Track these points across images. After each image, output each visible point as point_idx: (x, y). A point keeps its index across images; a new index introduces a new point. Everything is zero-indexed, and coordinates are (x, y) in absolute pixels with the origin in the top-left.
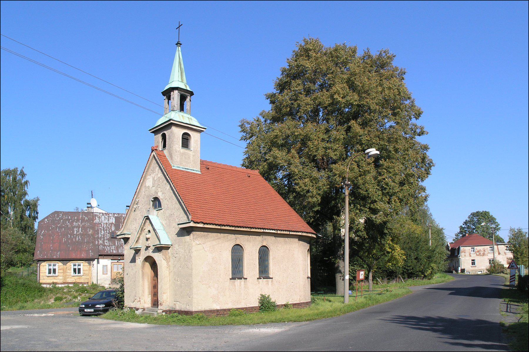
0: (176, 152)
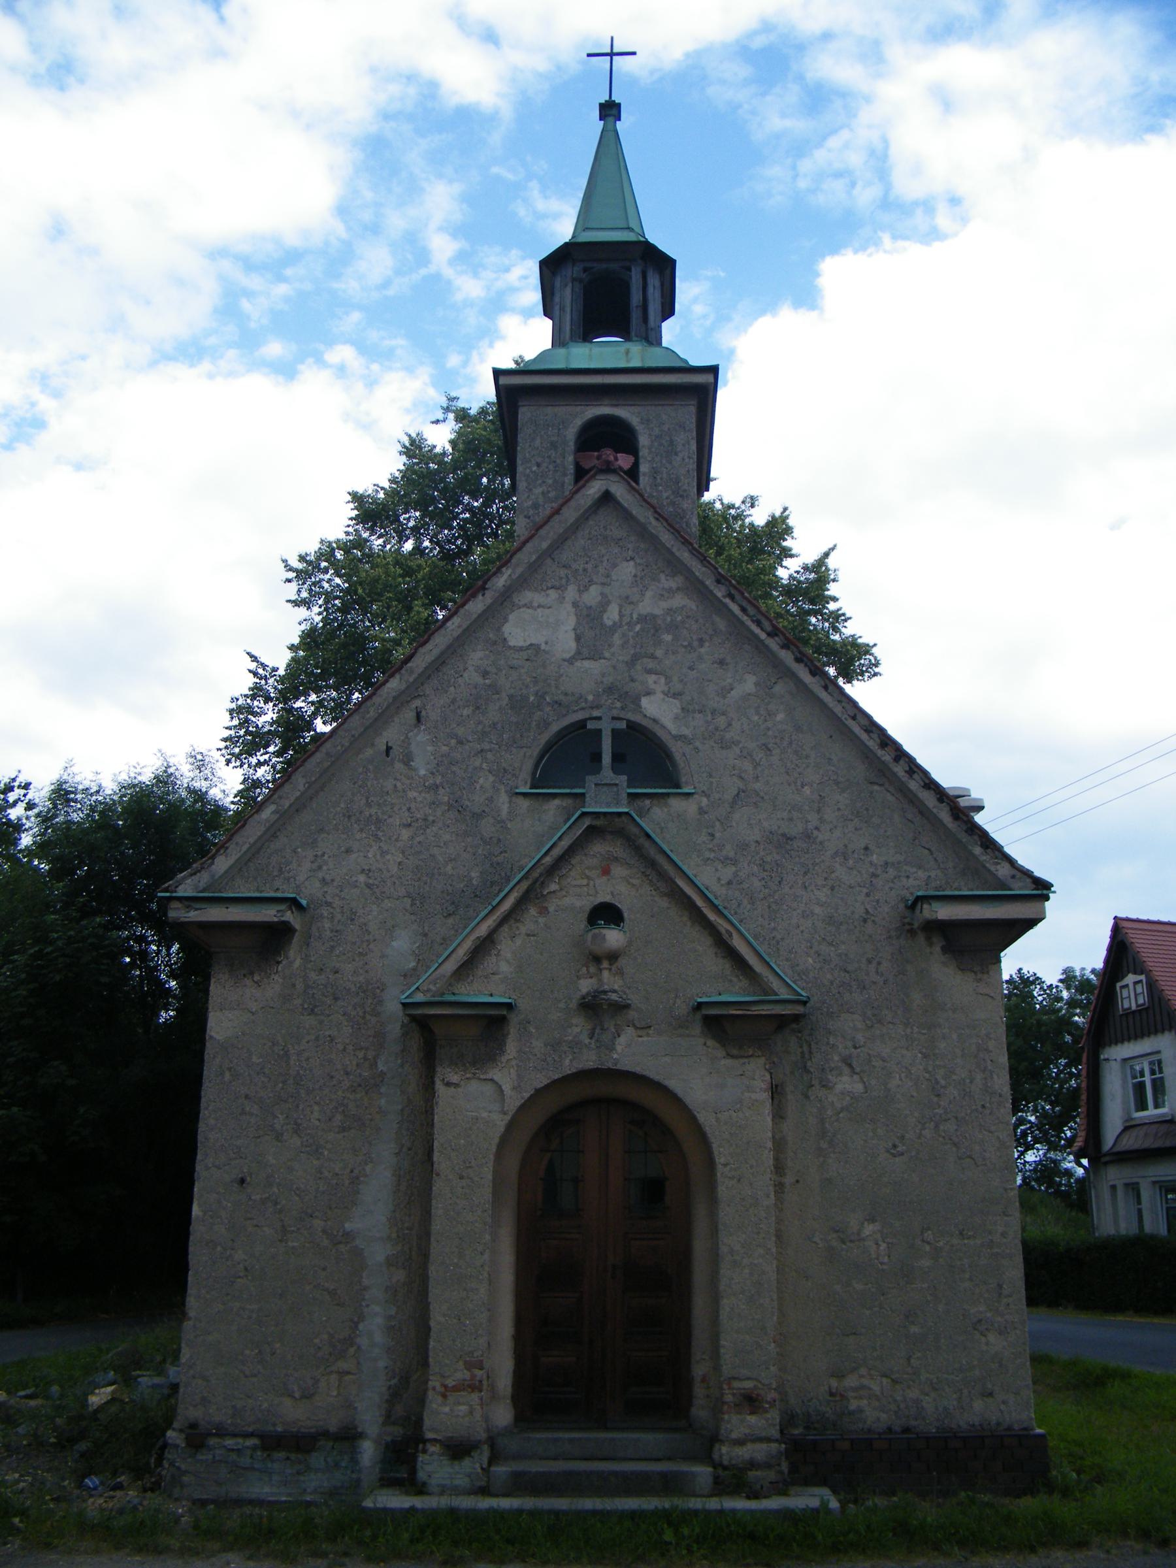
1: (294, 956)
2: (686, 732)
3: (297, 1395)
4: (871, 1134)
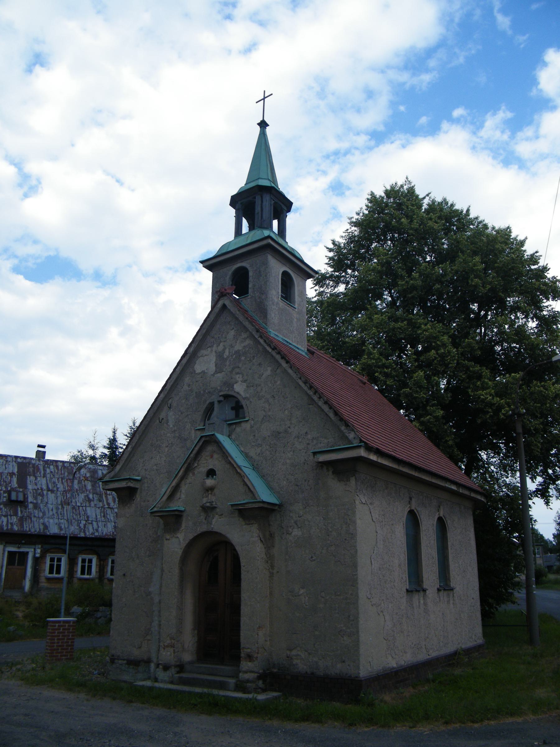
0: (273, 304)
1: (138, 497)
2: (248, 396)
3: (137, 647)
4: (304, 552)
